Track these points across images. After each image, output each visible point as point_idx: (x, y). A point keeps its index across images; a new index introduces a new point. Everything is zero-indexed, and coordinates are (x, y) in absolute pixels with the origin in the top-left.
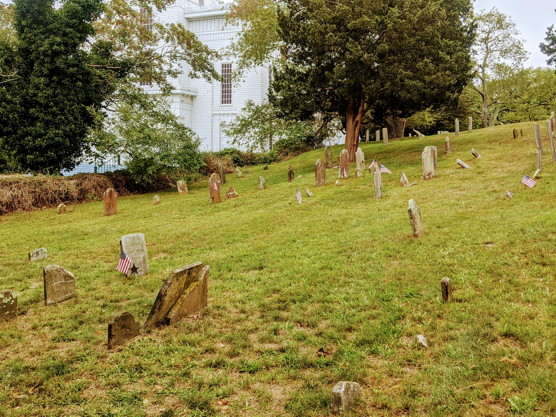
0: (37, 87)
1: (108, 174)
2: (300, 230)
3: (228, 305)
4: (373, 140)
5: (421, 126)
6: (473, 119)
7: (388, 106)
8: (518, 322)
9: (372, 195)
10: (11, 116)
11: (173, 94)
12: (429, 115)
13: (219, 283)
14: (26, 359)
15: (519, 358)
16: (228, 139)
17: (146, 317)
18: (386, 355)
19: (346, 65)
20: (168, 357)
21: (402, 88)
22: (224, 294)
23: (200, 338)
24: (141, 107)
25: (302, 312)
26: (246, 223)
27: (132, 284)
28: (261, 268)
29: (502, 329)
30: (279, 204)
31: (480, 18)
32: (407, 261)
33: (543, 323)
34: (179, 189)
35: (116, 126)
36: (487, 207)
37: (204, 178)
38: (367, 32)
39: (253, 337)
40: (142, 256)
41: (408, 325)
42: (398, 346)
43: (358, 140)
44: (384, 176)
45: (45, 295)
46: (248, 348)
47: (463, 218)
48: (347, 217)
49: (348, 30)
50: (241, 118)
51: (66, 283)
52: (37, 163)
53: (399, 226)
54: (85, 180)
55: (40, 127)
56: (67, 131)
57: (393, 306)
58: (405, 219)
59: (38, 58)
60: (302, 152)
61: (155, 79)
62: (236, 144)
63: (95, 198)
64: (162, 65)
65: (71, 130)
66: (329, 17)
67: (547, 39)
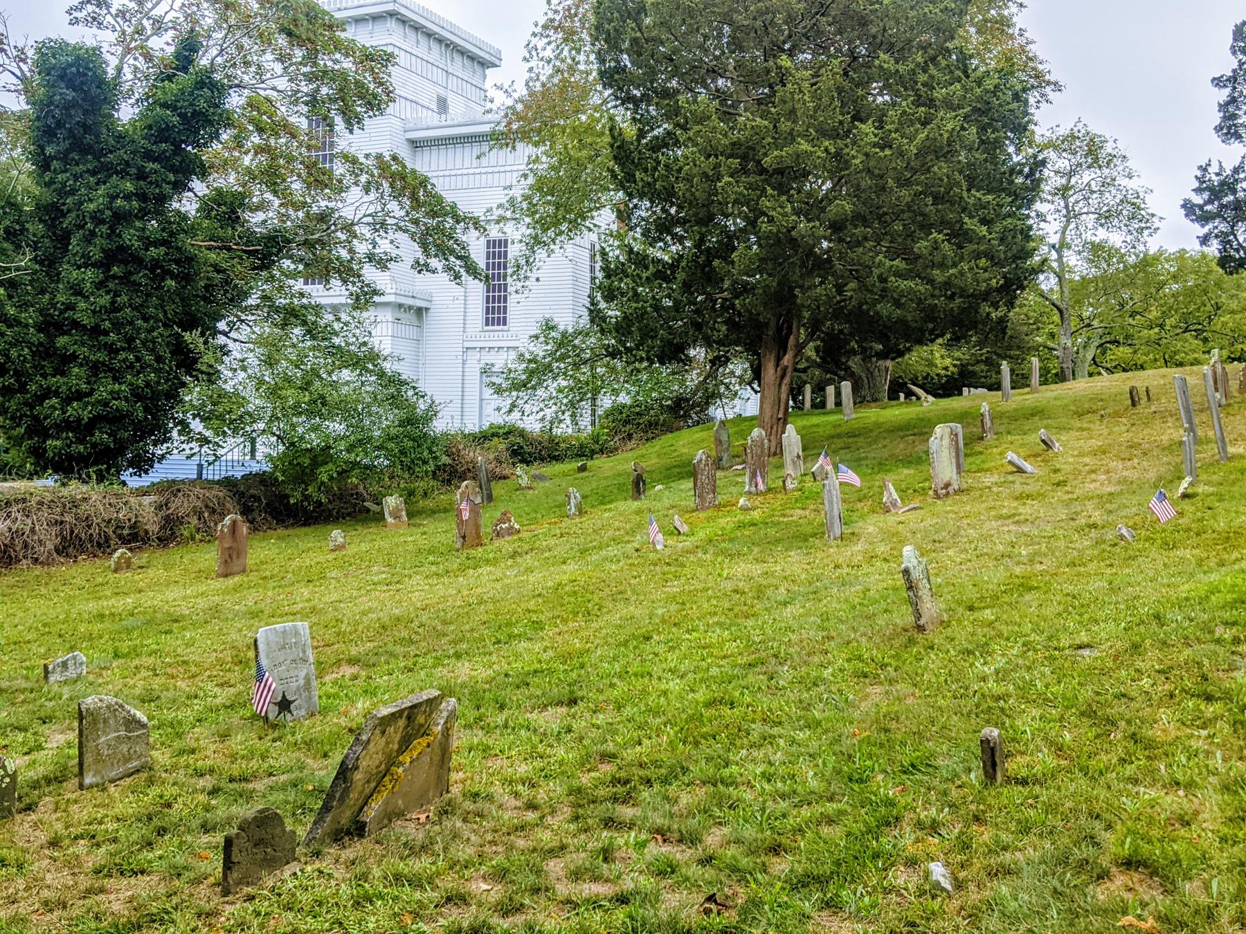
0: (77, 290)
1: (228, 483)
2: (660, 612)
3: (497, 789)
4: (819, 405)
5: (925, 378)
6: (1041, 360)
7: (852, 334)
8: (1155, 833)
9: (820, 532)
10: (14, 353)
11: (376, 304)
12: (943, 352)
13: (478, 737)
14: (34, 917)
15: (1160, 917)
16: (496, 401)
17: (310, 819)
18: (859, 911)
19: (760, 246)
20: (359, 914)
21: (882, 297)
22: (487, 764)
23: (434, 868)
24: (305, 335)
25: (667, 806)
26: (539, 595)
27: (280, 739)
28: (573, 702)
29: (1120, 849)
30: (612, 551)
31: (1051, 145)
32: (902, 688)
33: (1210, 834)
34: (387, 515)
35: (249, 377)
36: (1077, 562)
37: (443, 490)
38: (806, 174)
39: (555, 867)
40: (303, 674)
41: (907, 839)
42: (885, 889)
43: (786, 409)
44: (847, 489)
45: (81, 764)
46: (542, 895)
47: (1026, 586)
48: (765, 583)
49: (763, 171)
50: (527, 356)
51: (129, 738)
52: (70, 457)
53: (883, 605)
54: (175, 495)
55: (79, 378)
56: (138, 387)
57: (872, 793)
58: (895, 589)
59: (82, 227)
60: (664, 432)
61: (339, 271)
62: (516, 415)
63: (198, 537)
64: (355, 241)
65: (148, 385)
66: (725, 141)
67: (1198, 191)
